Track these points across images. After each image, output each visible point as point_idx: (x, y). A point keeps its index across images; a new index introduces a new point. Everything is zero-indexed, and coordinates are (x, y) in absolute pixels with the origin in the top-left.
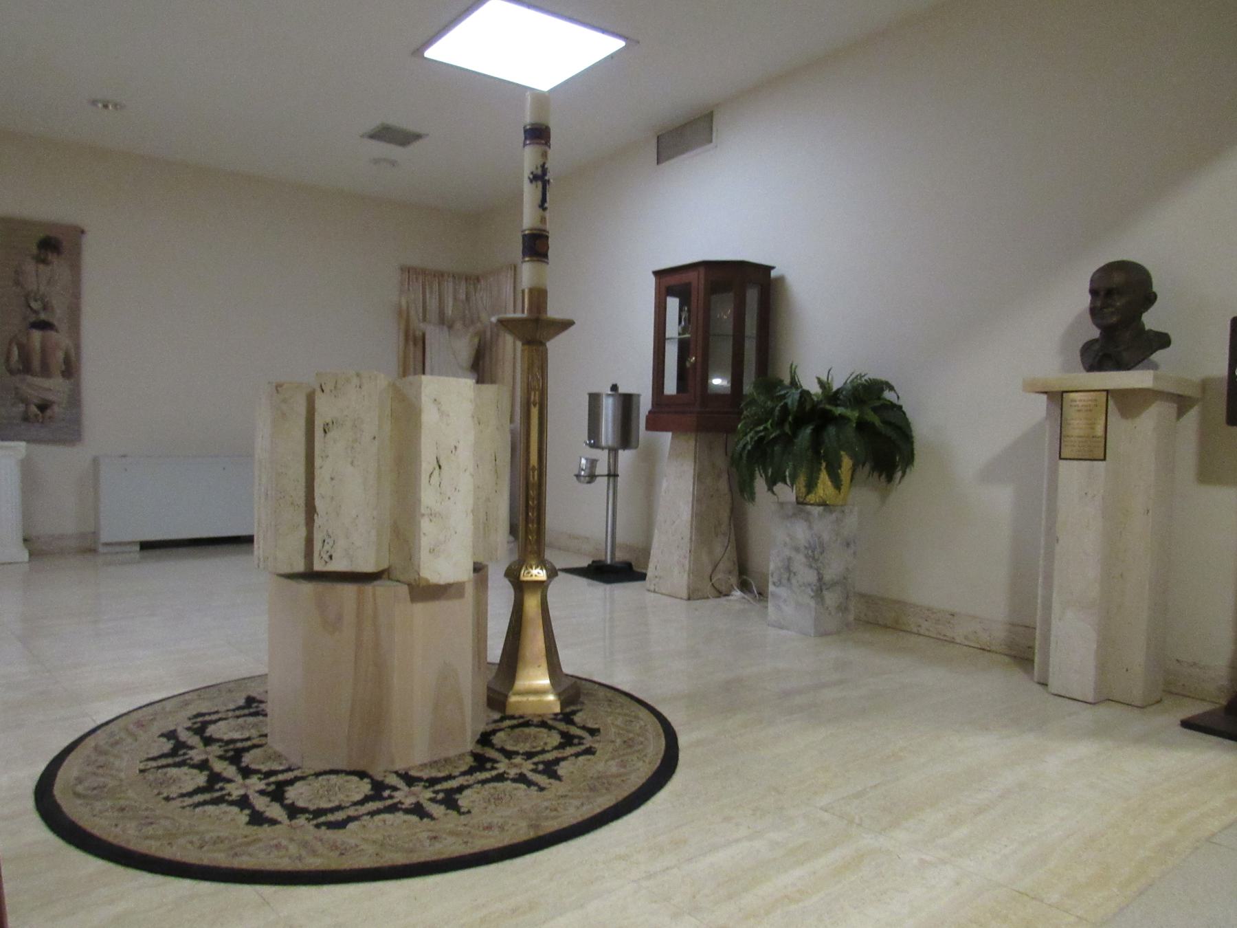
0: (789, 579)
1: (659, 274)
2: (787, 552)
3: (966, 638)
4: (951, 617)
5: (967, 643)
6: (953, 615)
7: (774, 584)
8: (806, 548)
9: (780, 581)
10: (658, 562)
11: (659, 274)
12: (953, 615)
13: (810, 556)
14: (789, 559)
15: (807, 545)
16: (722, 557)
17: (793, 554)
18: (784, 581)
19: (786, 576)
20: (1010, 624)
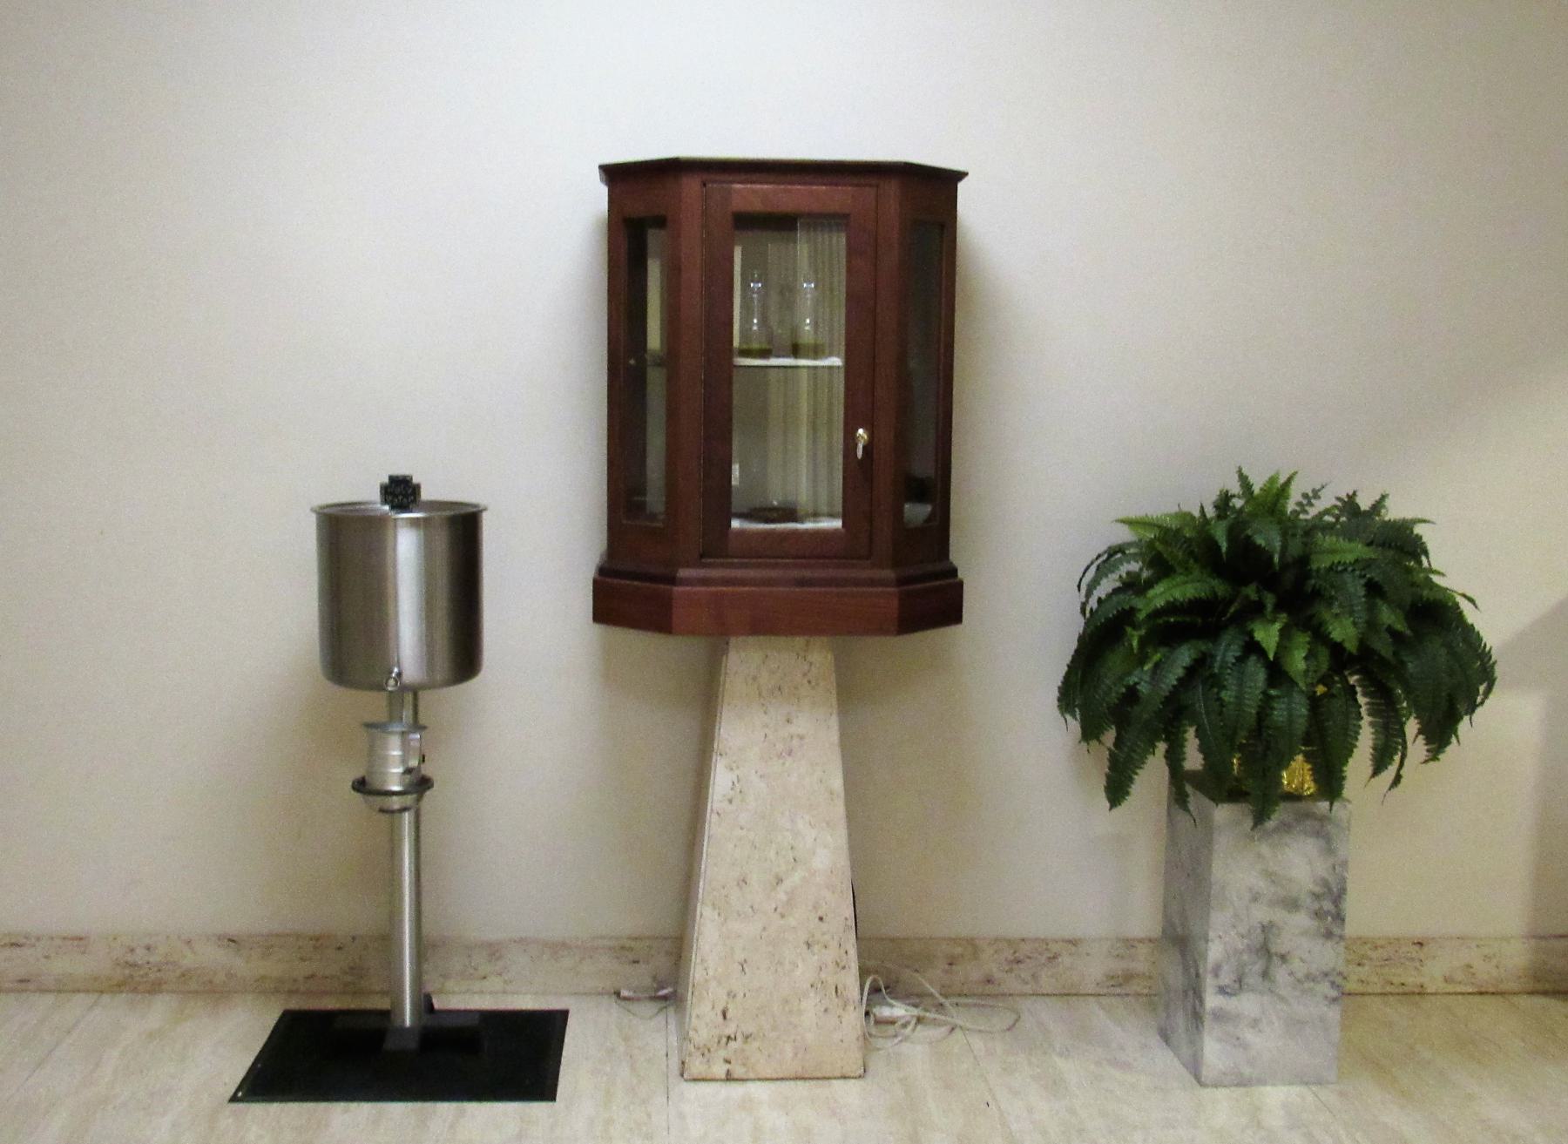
0: (1265, 974)
1: (615, 175)
2: (1261, 914)
3: (1447, 980)
4: (1417, 948)
5: (1450, 988)
6: (1420, 944)
7: (1222, 990)
8: (1316, 896)
9: (1240, 980)
10: (731, 995)
11: (615, 175)
12: (1420, 944)
13: (1328, 913)
14: (1267, 929)
15: (1317, 889)
16: (1391, 994)
17: (1279, 915)
18: (1253, 979)
19: (1258, 967)
20: (1534, 937)
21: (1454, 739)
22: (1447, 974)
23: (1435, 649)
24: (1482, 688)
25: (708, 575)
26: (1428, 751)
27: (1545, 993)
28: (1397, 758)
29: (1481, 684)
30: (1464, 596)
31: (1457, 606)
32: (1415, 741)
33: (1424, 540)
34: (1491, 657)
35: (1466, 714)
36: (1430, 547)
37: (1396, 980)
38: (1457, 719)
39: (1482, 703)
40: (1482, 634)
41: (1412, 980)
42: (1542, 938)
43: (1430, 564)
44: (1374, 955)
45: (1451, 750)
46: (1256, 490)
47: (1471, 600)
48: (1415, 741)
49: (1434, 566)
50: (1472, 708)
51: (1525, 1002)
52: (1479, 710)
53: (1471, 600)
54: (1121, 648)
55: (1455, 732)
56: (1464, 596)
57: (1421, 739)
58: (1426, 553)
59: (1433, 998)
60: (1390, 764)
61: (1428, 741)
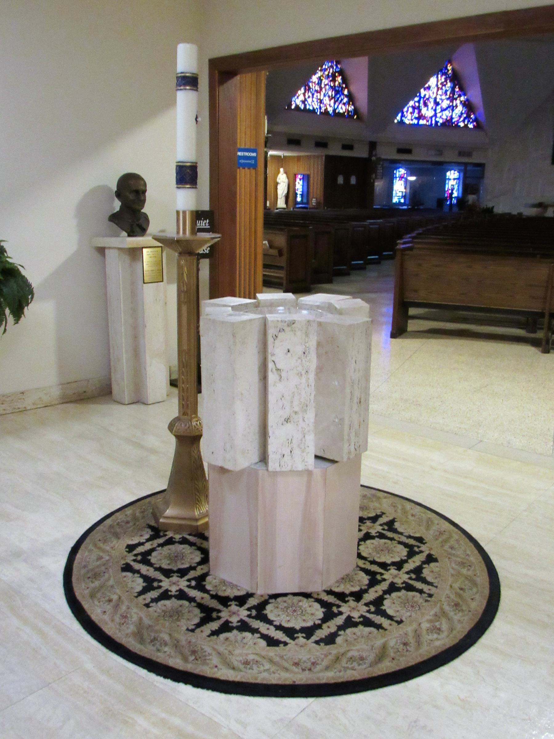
3: (34, 404)
21: (23, 316)
22: (33, 402)
23: (12, 284)
24: (30, 297)
25: (237, 238)
26: (15, 320)
27: (67, 403)
28: (4, 323)
29: (30, 295)
30: (20, 265)
31: (18, 270)
32: (9, 316)
33: (5, 247)
34: (32, 286)
35: (26, 306)
36: (7, 250)
37: (16, 407)
38: (23, 308)
39: (31, 302)
40: (28, 279)
41: (21, 406)
42: (63, 384)
43: (7, 255)
44: (7, 400)
45: (23, 319)
46: (435, 76)
47: (23, 267)
48: (9, 316)
49: (9, 255)
50: (28, 305)
51: (59, 406)
52: (30, 305)
53: (23, 267)
54: (100, 561)
55: (23, 313)
56: (20, 265)
57: (11, 316)
58: (6, 252)
59: (29, 411)
60: (2, 325)
61: (14, 316)
